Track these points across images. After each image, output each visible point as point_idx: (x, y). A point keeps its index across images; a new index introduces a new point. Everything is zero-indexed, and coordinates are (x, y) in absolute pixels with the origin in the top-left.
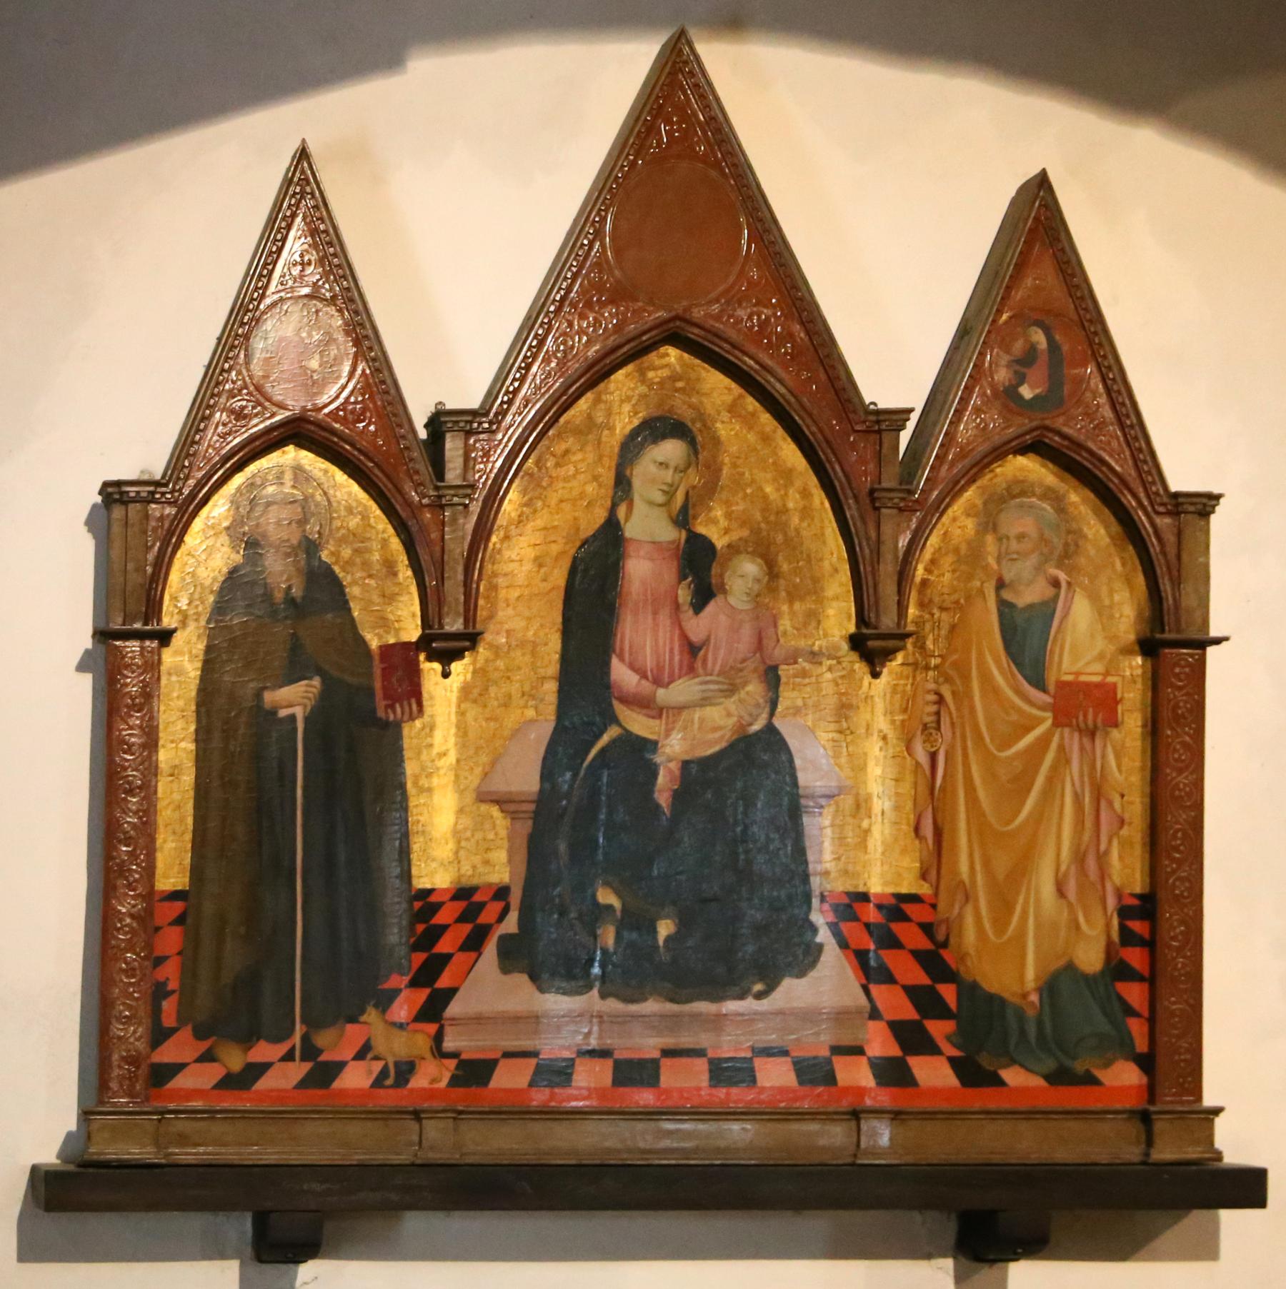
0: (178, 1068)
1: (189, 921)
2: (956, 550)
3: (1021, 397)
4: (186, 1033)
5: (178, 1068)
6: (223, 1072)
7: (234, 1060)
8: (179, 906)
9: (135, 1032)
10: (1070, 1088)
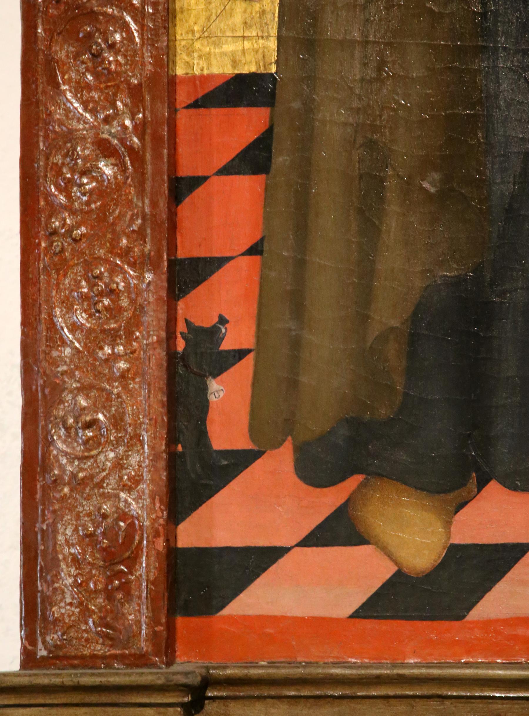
0: (257, 560)
1: (280, 160)
2: (516, 271)
3: (108, 587)
4: (280, 462)
5: (257, 560)
6: (386, 571)
7: (414, 534)
8: (246, 124)
9: (119, 465)
10: (248, 143)
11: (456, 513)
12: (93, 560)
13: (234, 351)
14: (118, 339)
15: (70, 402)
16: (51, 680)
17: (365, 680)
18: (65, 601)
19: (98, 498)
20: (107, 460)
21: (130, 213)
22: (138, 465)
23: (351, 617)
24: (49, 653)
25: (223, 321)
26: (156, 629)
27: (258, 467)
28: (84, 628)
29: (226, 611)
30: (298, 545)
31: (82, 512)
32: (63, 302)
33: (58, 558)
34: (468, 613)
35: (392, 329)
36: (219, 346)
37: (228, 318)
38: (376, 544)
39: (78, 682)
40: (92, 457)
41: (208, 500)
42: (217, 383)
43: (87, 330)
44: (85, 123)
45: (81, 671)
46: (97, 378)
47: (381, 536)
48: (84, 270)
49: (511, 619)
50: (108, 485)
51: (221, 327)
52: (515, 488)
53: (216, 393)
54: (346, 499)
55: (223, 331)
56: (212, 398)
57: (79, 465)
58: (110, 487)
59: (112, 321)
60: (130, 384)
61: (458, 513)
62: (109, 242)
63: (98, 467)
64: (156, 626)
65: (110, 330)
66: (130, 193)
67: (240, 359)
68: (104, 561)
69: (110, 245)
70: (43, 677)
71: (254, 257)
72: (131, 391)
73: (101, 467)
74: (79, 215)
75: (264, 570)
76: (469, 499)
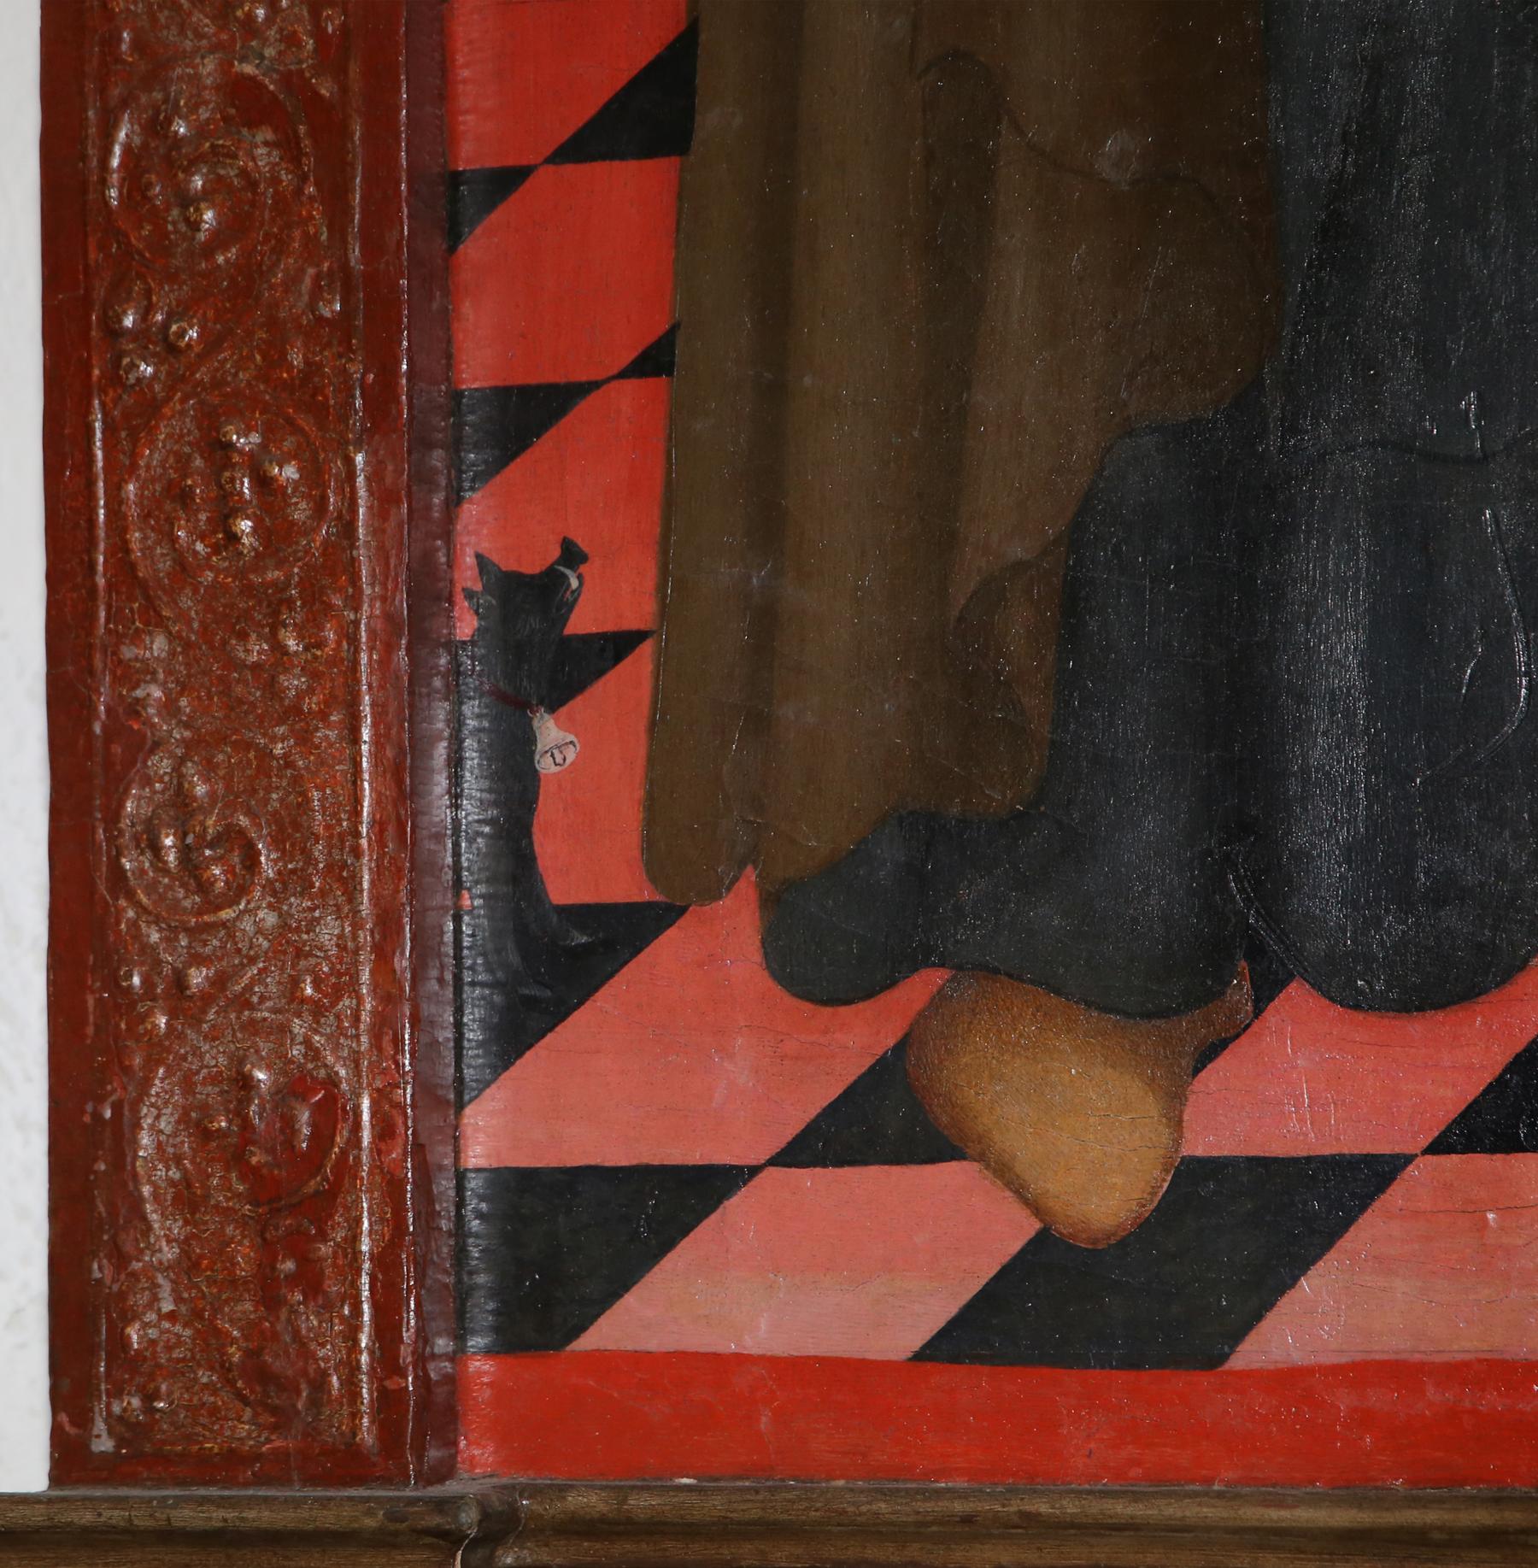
0: (667, 1203)
1: (719, 118)
4: (722, 942)
5: (667, 1203)
6: (1011, 1232)
7: (1086, 1134)
9: (289, 945)
11: (1197, 1071)
12: (228, 1199)
13: (603, 636)
14: (284, 609)
15: (166, 779)
16: (100, 1515)
17: (934, 1528)
18: (159, 1309)
19: (239, 1035)
20: (259, 931)
21: (311, 271)
22: (338, 945)
23: (919, 1356)
24: (118, 1447)
25: (572, 555)
26: (387, 1383)
27: (669, 951)
28: (205, 1380)
29: (588, 1341)
30: (773, 1162)
31: (198, 1072)
32: (149, 515)
33: (140, 1193)
34: (1232, 1350)
35: (1019, 567)
36: (564, 625)
37: (586, 550)
38: (981, 1158)
39: (169, 1519)
40: (224, 924)
41: (538, 1040)
42: (557, 724)
43: (206, 588)
44: (200, 36)
45: (177, 1492)
46: (233, 715)
47: (997, 1136)
48: (199, 428)
49: (1354, 1366)
50: (262, 999)
51: (568, 572)
52: (1355, 1002)
53: (556, 752)
54: (900, 1035)
55: (574, 583)
56: (545, 766)
57: (189, 947)
58: (269, 1004)
59: (270, 562)
60: (317, 729)
61: (1203, 1074)
62: (261, 351)
63: (239, 951)
64: (389, 1377)
65: (266, 585)
66: (312, 218)
67: (618, 658)
68: (256, 1203)
69: (264, 358)
70: (99, 1506)
71: (652, 382)
72: (318, 747)
73: (244, 951)
74: (184, 282)
75: (686, 1231)
76: (1232, 1032)
